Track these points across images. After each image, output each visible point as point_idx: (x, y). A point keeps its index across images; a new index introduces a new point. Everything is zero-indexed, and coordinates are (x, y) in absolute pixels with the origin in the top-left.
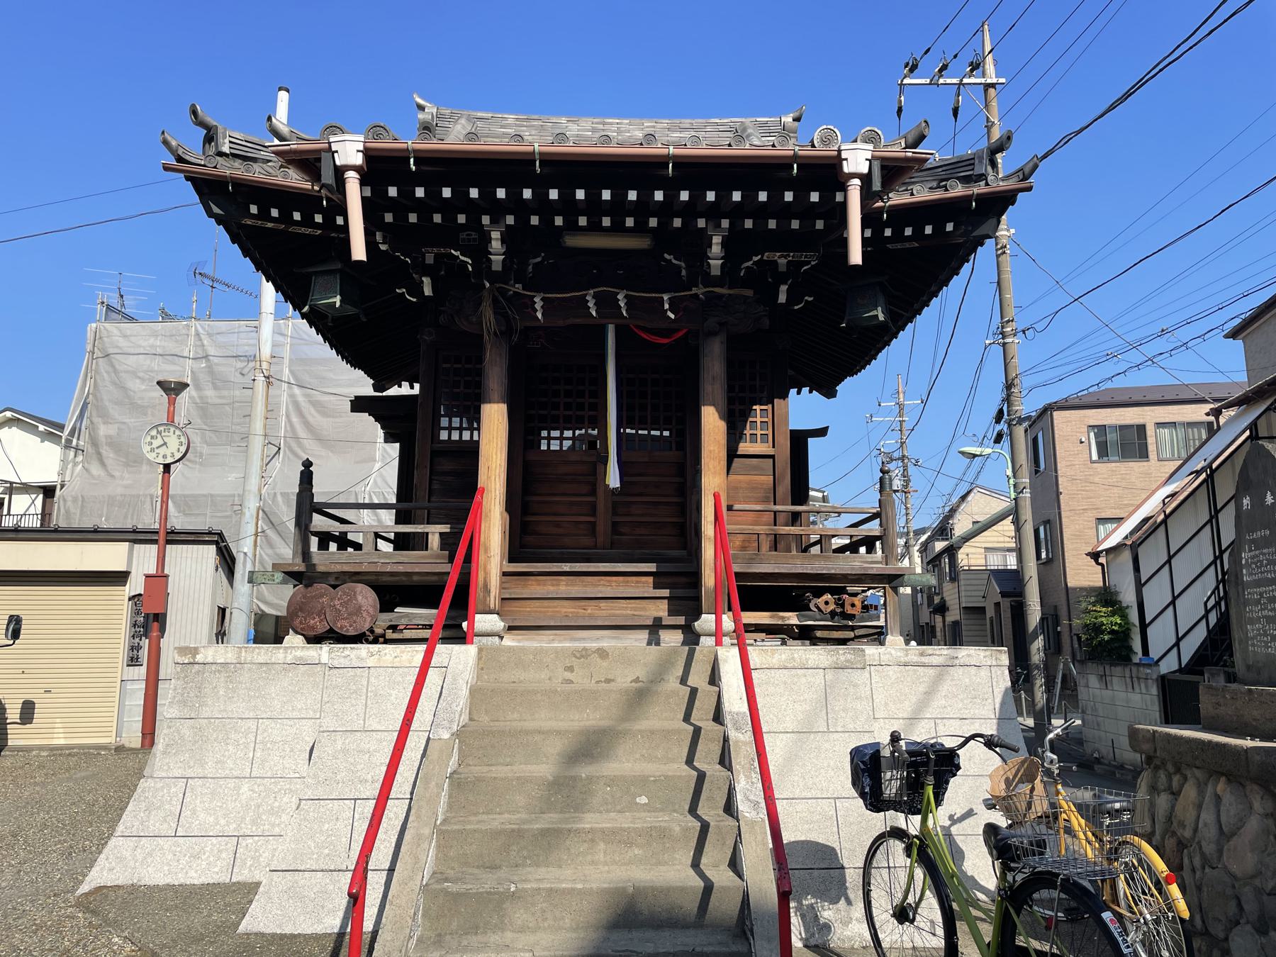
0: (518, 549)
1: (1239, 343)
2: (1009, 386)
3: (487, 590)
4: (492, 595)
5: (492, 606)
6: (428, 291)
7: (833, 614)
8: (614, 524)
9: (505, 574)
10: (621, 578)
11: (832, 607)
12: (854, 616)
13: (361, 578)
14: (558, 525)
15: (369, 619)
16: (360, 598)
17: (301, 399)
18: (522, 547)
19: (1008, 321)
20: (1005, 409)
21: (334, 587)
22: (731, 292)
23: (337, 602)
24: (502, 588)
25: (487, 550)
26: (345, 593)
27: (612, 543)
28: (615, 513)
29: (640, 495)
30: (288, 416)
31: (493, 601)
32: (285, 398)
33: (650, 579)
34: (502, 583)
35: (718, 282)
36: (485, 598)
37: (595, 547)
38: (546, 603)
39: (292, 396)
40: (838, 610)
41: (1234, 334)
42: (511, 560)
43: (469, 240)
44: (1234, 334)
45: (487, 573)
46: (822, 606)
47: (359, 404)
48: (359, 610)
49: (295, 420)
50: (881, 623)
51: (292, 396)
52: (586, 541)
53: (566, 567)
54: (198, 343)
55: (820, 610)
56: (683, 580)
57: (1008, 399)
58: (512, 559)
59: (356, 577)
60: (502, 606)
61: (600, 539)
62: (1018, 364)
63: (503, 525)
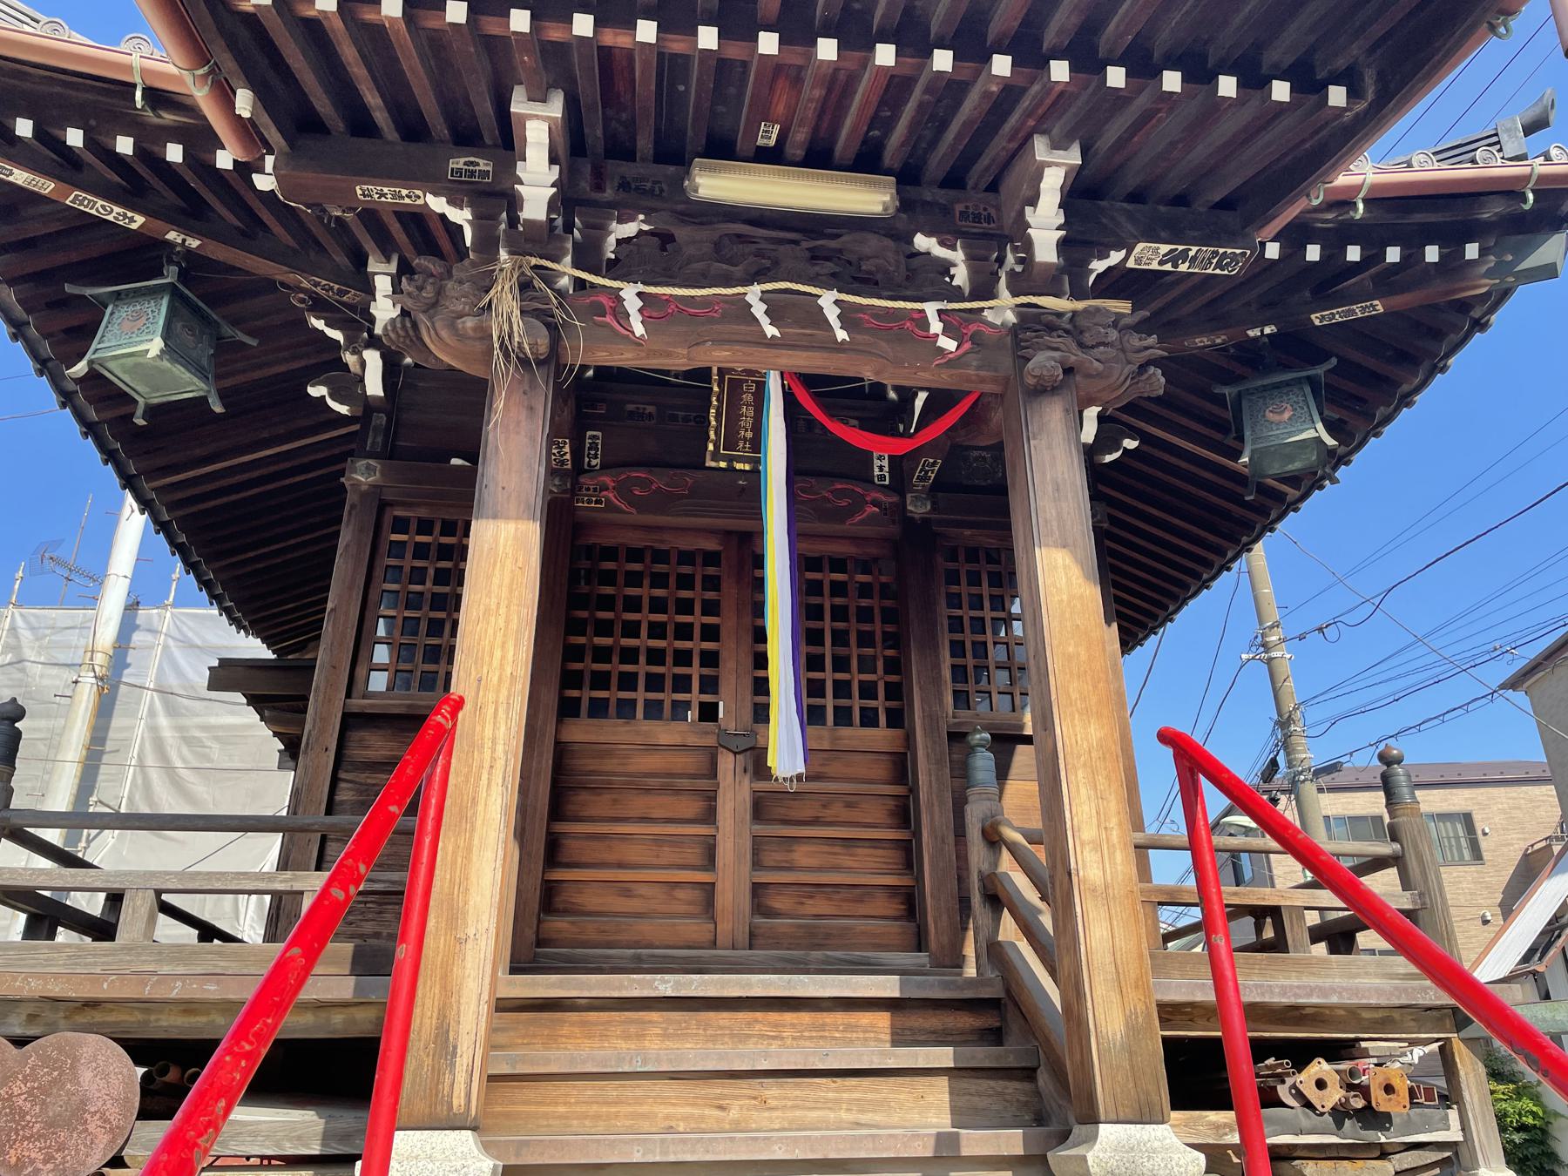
0: (546, 929)
1: (1519, 697)
2: (1284, 723)
3: (445, 1048)
4: (462, 1062)
5: (458, 1101)
6: (374, 386)
7: (1340, 1114)
8: (757, 889)
9: (503, 1006)
10: (805, 1017)
11: (1334, 1095)
12: (1387, 1117)
13: (97, 1016)
14: (625, 889)
15: (103, 1139)
16: (86, 1076)
17: (167, 734)
18: (540, 943)
19: (1272, 627)
20: (1281, 759)
21: (20, 1042)
22: (1080, 305)
23: (18, 1088)
24: (491, 1046)
25: (455, 917)
26: (45, 1061)
27: (752, 935)
28: (757, 864)
29: (815, 822)
30: (141, 765)
31: (463, 1086)
32: (140, 729)
33: (883, 1020)
34: (492, 1030)
35: (1049, 282)
36: (437, 1074)
37: (714, 944)
38: (612, 1089)
39: (154, 729)
40: (1359, 1103)
41: (1514, 683)
42: (520, 965)
43: (472, 173)
44: (1514, 683)
45: (449, 993)
46: (1311, 1093)
47: (227, 675)
48: (77, 1114)
49: (150, 760)
50: (1454, 1134)
51: (154, 729)
52: (695, 929)
53: (666, 985)
54: (12, 641)
55: (1308, 1105)
56: (966, 1021)
57: (1286, 744)
58: (520, 965)
59: (84, 1011)
60: (487, 1100)
61: (724, 927)
62: (1293, 692)
63: (772, 178)
